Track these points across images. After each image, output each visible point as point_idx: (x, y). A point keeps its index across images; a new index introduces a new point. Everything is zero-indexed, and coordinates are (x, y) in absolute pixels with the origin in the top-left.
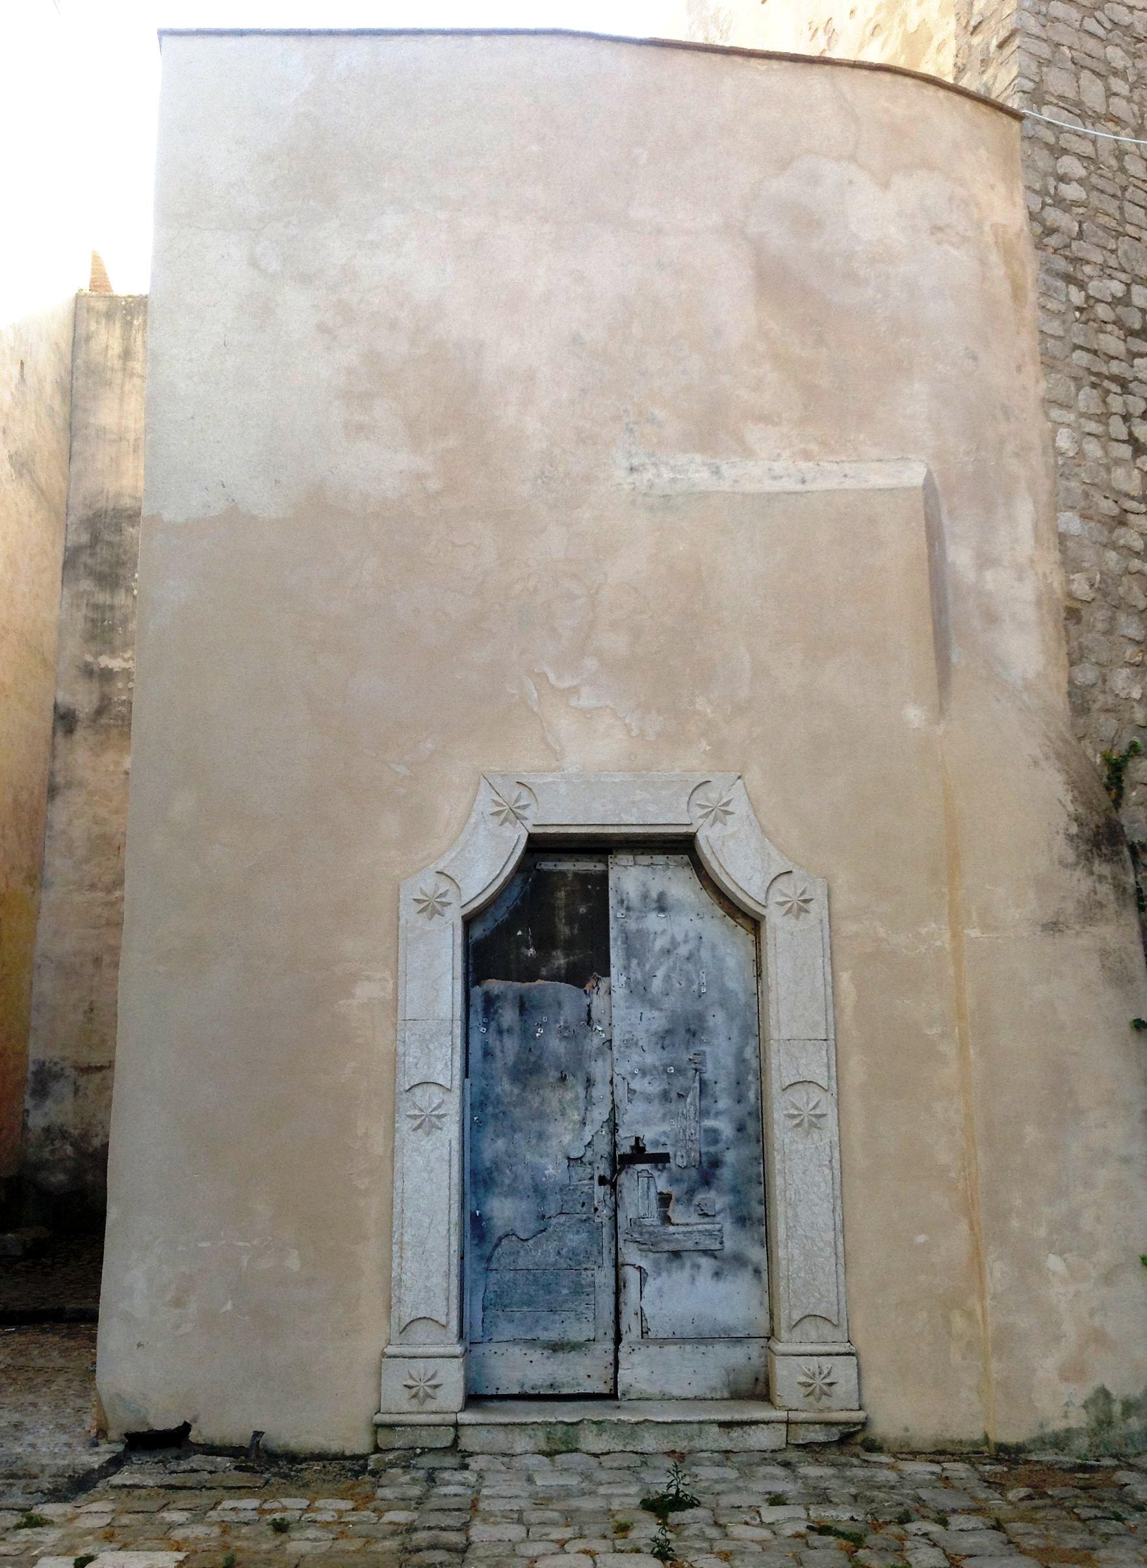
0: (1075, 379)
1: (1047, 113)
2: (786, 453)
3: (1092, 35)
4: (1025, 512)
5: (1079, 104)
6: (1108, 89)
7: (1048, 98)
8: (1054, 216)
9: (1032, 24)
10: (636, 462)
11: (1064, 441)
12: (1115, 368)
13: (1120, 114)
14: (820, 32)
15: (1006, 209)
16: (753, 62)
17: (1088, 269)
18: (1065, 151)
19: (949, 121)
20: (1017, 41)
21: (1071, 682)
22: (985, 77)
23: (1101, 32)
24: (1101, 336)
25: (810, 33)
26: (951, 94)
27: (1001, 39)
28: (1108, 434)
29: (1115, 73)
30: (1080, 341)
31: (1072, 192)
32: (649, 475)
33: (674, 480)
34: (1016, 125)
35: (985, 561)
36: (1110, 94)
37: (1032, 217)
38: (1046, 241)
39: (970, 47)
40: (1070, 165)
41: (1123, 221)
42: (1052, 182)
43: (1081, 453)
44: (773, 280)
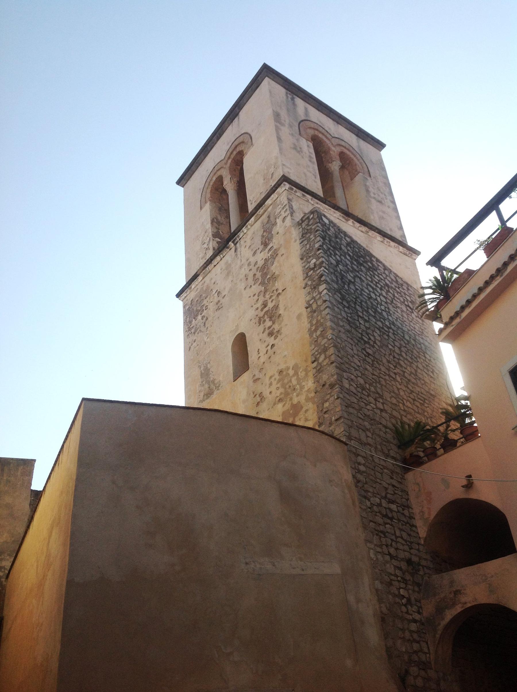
0: (372, 532)
1: (353, 443)
2: (294, 559)
3: (360, 418)
4: (366, 580)
5: (360, 440)
6: (366, 435)
7: (352, 438)
8: (359, 476)
9: (346, 415)
10: (247, 561)
11: (372, 556)
12: (382, 528)
13: (370, 443)
14: (257, 396)
15: (347, 475)
16: (273, 424)
17: (369, 494)
18: (358, 455)
19: (330, 447)
20: (342, 420)
21: (386, 645)
22: (331, 428)
23: (362, 417)
24: (376, 517)
25: (254, 395)
26: (329, 437)
27: (336, 418)
28: (383, 552)
29: (367, 430)
30: (371, 519)
31: (362, 468)
32: (252, 566)
33: (261, 568)
34: (346, 447)
35: (358, 601)
36: (367, 437)
37: (354, 477)
38: (358, 484)
39: (324, 417)
40: (360, 459)
41: (376, 478)
42: (357, 465)
43: (377, 559)
44: (285, 496)
